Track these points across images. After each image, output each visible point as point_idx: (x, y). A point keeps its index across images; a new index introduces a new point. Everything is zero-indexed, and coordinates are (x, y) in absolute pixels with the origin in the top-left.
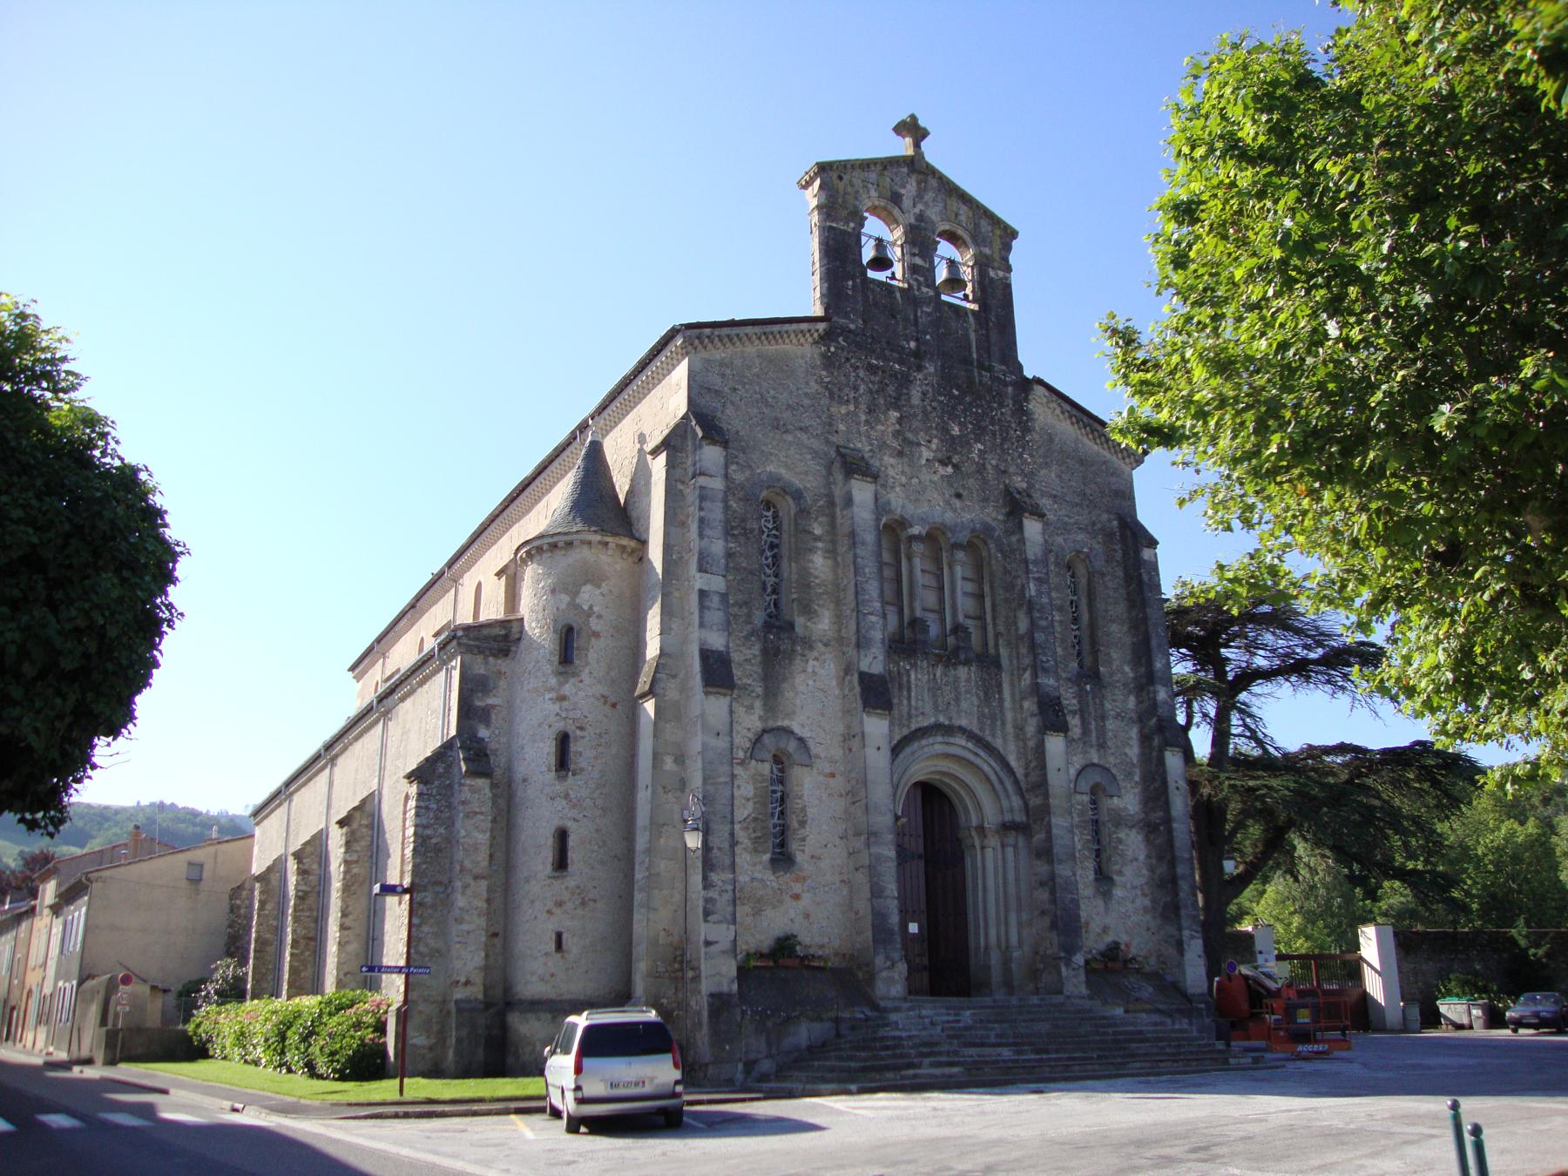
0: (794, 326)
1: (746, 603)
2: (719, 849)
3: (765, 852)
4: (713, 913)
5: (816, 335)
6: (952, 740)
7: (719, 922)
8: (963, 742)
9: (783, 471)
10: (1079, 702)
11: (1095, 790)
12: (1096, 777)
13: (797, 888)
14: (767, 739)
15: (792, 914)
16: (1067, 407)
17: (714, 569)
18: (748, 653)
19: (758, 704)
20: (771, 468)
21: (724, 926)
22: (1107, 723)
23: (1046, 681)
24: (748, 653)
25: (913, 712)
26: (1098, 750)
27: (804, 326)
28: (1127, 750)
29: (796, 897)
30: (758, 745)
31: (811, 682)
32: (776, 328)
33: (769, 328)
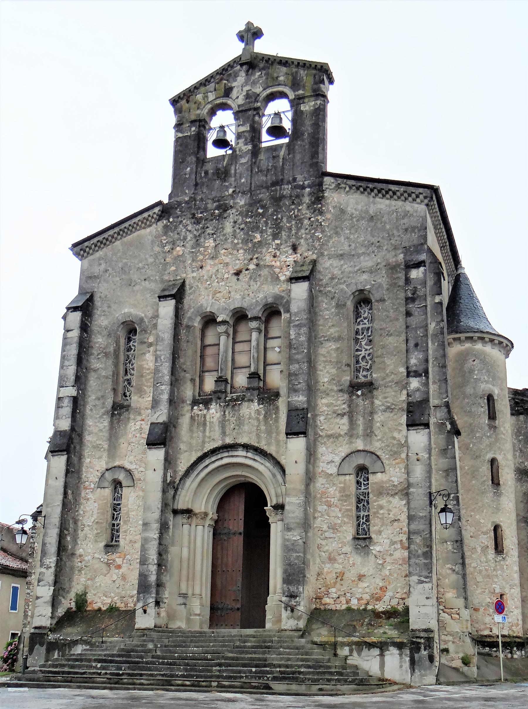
0: (140, 218)
1: (102, 396)
2: (50, 543)
3: (101, 542)
4: (43, 580)
5: (155, 216)
6: (235, 453)
7: (45, 586)
8: (244, 453)
9: (132, 310)
10: (349, 406)
11: (362, 470)
12: (360, 460)
13: (119, 561)
14: (107, 474)
15: (115, 577)
16: (351, 182)
17: (67, 384)
18: (101, 426)
19: (105, 454)
20: (126, 310)
21: (47, 587)
22: (376, 417)
23: (296, 398)
24: (101, 426)
25: (207, 440)
26: (364, 440)
27: (146, 215)
28: (396, 435)
29: (119, 567)
30: (102, 478)
31: (138, 435)
32: (126, 224)
33: (122, 226)
